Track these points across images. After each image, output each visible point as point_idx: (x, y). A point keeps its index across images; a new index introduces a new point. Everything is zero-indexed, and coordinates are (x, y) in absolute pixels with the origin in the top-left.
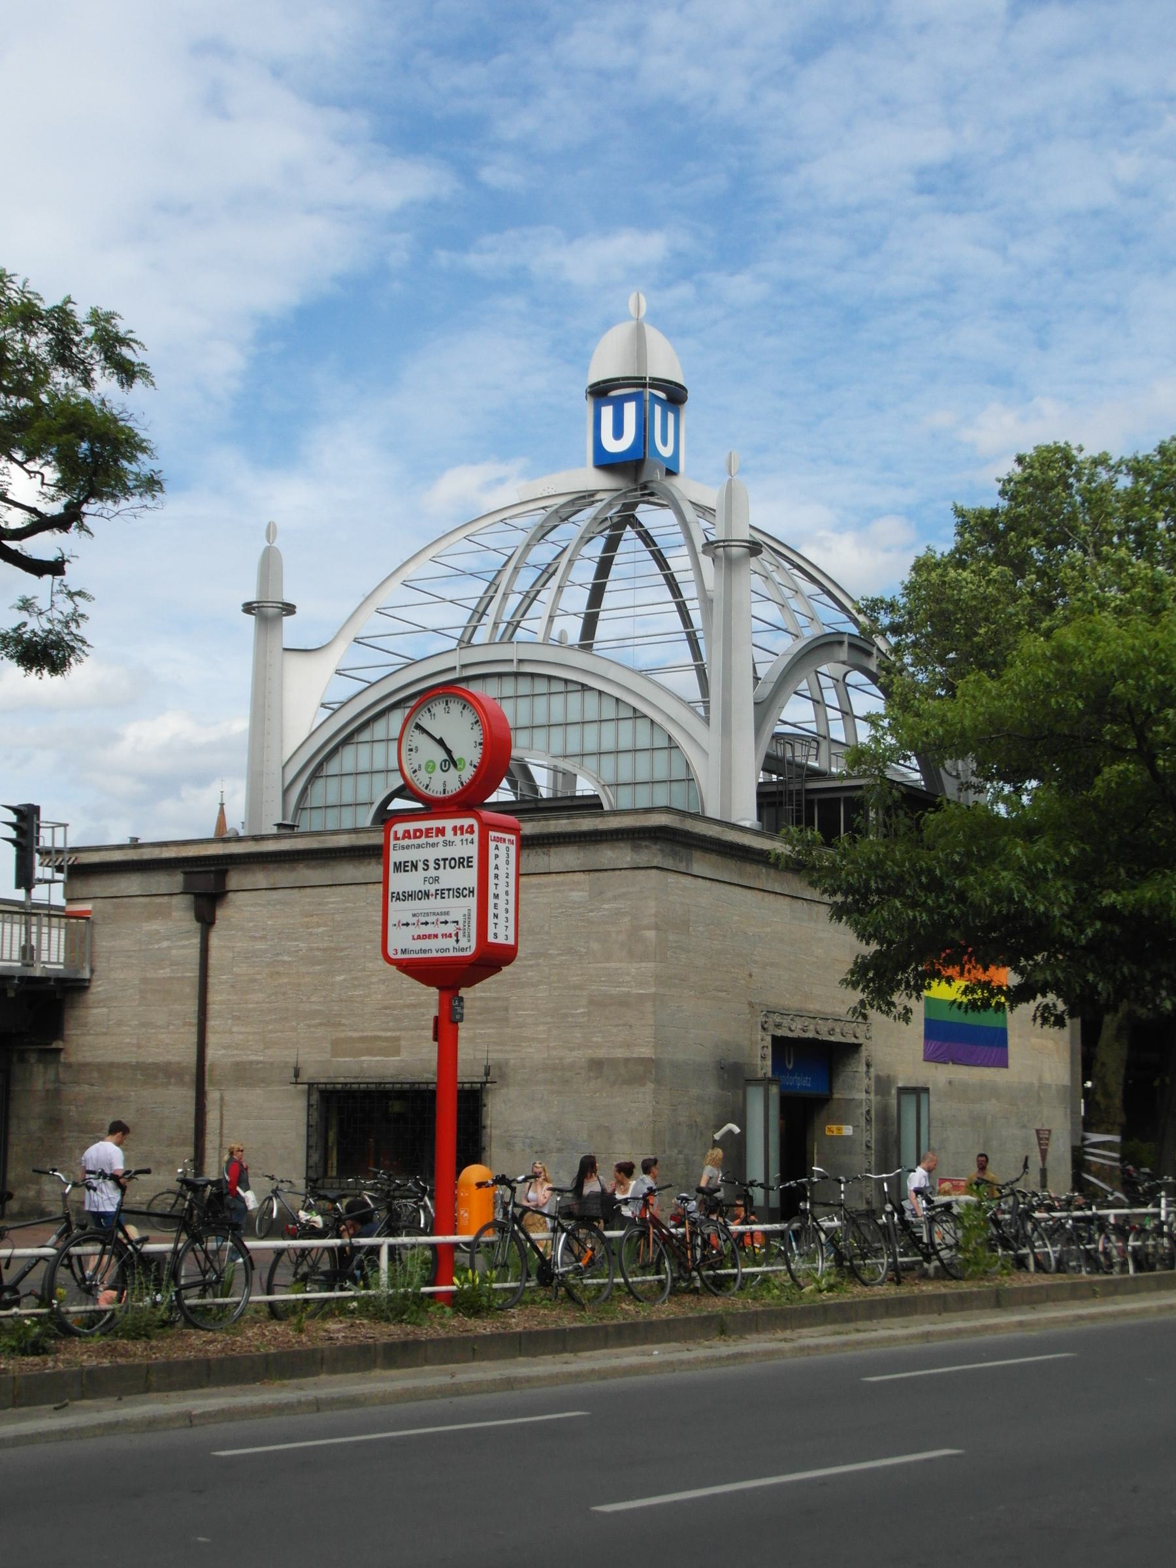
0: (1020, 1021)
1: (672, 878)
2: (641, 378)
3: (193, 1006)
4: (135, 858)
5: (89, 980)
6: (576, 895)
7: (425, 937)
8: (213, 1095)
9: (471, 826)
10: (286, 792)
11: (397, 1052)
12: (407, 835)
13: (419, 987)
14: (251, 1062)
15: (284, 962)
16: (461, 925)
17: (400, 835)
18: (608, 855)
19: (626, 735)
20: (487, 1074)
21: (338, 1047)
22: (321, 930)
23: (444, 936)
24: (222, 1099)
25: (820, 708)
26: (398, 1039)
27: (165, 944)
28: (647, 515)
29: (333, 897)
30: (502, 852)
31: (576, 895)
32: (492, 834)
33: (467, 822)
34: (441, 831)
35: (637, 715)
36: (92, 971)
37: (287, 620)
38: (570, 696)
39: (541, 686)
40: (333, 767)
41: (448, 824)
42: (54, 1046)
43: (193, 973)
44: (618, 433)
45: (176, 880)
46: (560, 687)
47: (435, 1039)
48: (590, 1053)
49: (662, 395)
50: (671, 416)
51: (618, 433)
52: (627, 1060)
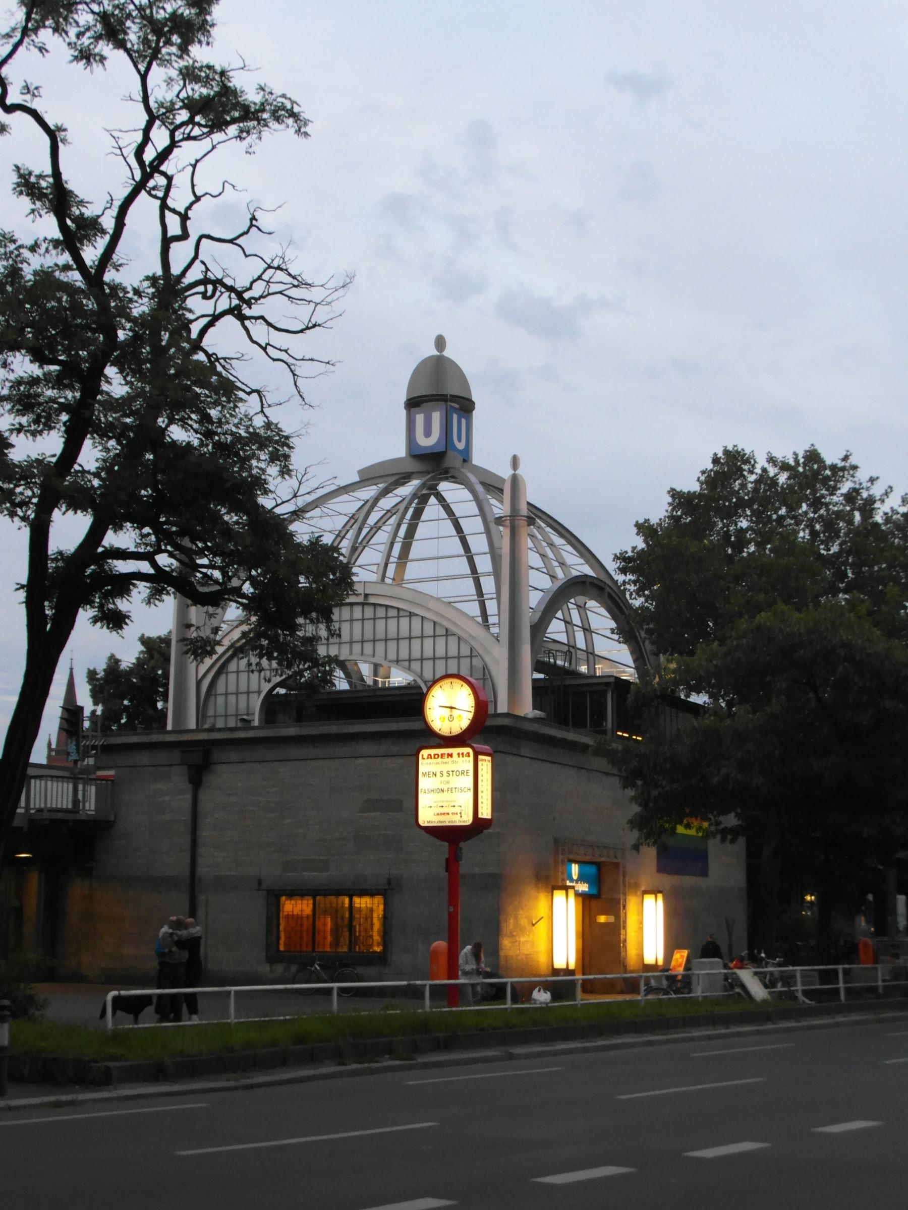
0: (714, 846)
1: (509, 759)
2: (444, 395)
3: (188, 839)
4: (147, 741)
5: (114, 822)
7: (441, 814)
8: (201, 898)
9: (468, 753)
10: (199, 683)
12: (429, 756)
13: (438, 842)
16: (463, 808)
17: (425, 756)
20: (389, 883)
22: (274, 790)
23: (453, 814)
25: (569, 627)
27: (167, 798)
28: (444, 487)
30: (484, 767)
32: (480, 757)
33: (466, 750)
34: (450, 755)
35: (448, 633)
36: (116, 816)
41: (455, 751)
43: (187, 817)
45: (176, 755)
47: (447, 871)
49: (456, 406)
50: (464, 421)
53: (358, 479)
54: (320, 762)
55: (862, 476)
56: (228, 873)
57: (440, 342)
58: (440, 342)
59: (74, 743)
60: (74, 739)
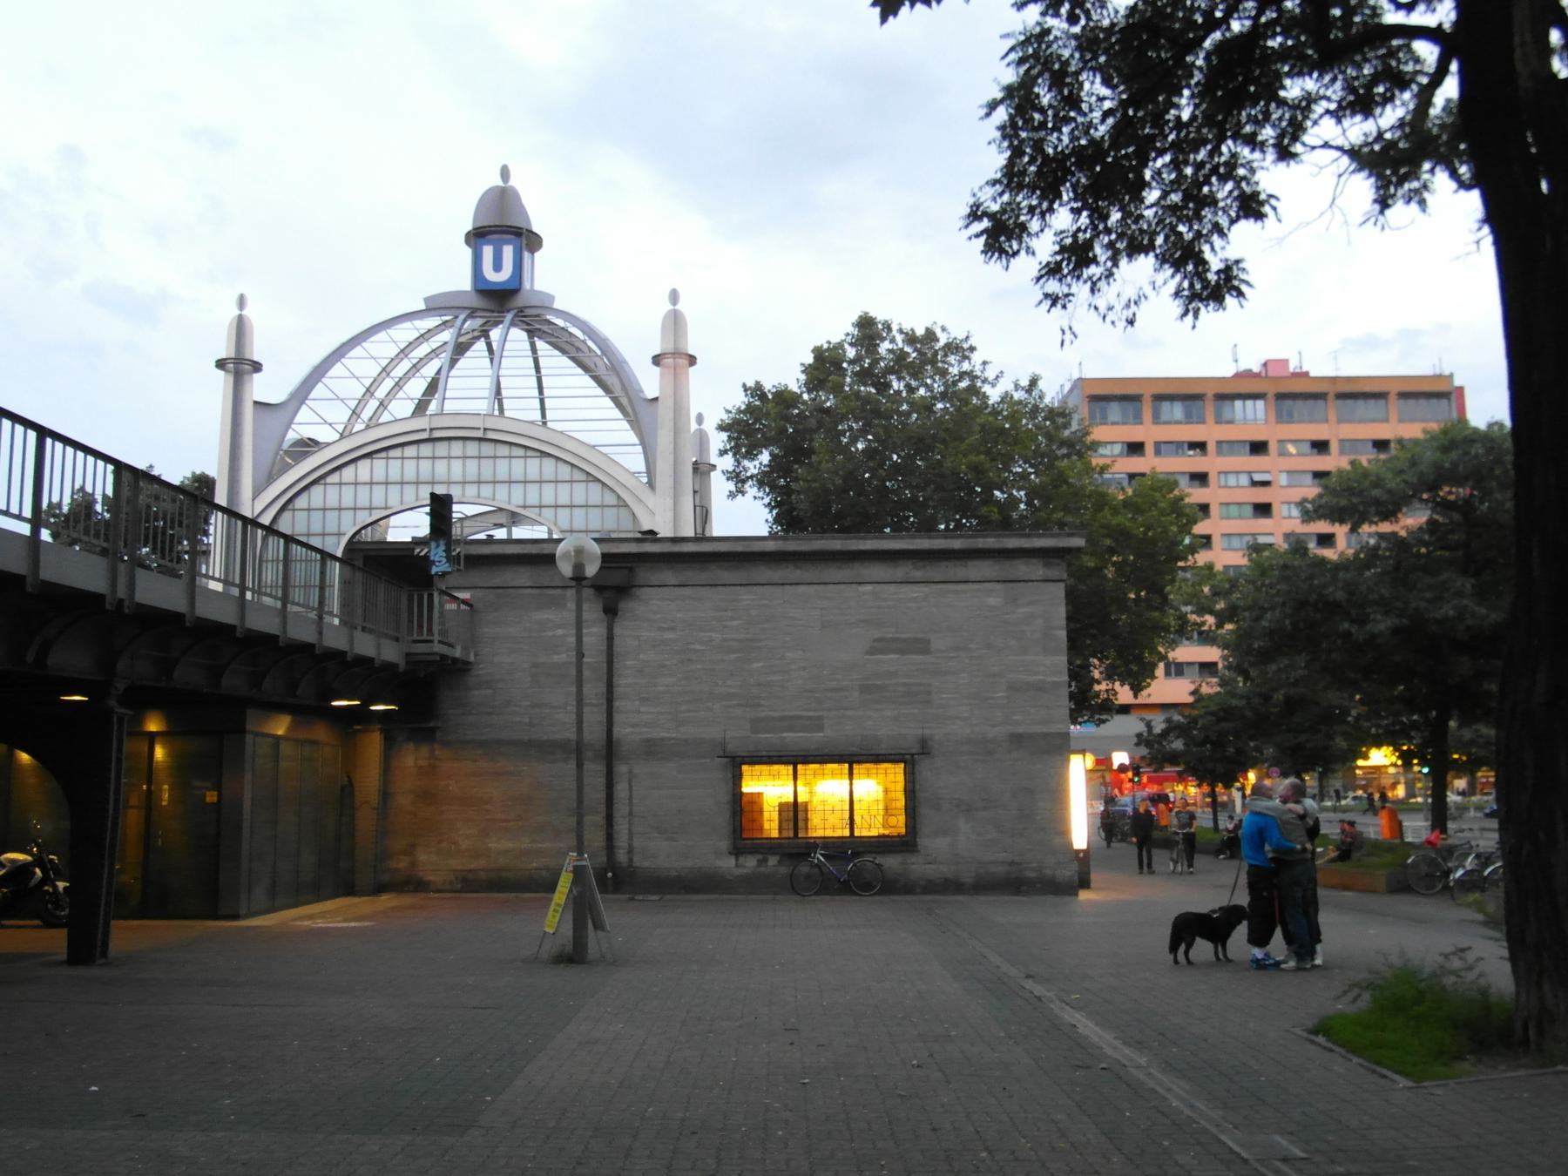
6: (992, 601)
8: (621, 769)
11: (821, 728)
14: (663, 739)
15: (697, 651)
18: (1022, 568)
19: (580, 493)
21: (757, 725)
22: (735, 623)
24: (630, 772)
26: (820, 718)
27: (560, 632)
29: (747, 597)
31: (992, 601)
36: (476, 655)
37: (256, 376)
38: (529, 461)
39: (503, 450)
40: (301, 502)
42: (432, 724)
44: (498, 267)
46: (521, 452)
48: (1011, 729)
51: (498, 267)
52: (1046, 735)
53: (423, 307)
54: (802, 589)
55: (977, 358)
56: (665, 735)
57: (505, 173)
58: (505, 173)
59: (442, 547)
60: (442, 542)
